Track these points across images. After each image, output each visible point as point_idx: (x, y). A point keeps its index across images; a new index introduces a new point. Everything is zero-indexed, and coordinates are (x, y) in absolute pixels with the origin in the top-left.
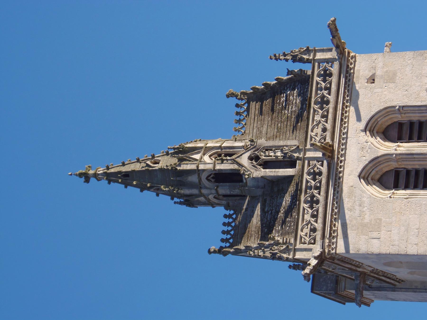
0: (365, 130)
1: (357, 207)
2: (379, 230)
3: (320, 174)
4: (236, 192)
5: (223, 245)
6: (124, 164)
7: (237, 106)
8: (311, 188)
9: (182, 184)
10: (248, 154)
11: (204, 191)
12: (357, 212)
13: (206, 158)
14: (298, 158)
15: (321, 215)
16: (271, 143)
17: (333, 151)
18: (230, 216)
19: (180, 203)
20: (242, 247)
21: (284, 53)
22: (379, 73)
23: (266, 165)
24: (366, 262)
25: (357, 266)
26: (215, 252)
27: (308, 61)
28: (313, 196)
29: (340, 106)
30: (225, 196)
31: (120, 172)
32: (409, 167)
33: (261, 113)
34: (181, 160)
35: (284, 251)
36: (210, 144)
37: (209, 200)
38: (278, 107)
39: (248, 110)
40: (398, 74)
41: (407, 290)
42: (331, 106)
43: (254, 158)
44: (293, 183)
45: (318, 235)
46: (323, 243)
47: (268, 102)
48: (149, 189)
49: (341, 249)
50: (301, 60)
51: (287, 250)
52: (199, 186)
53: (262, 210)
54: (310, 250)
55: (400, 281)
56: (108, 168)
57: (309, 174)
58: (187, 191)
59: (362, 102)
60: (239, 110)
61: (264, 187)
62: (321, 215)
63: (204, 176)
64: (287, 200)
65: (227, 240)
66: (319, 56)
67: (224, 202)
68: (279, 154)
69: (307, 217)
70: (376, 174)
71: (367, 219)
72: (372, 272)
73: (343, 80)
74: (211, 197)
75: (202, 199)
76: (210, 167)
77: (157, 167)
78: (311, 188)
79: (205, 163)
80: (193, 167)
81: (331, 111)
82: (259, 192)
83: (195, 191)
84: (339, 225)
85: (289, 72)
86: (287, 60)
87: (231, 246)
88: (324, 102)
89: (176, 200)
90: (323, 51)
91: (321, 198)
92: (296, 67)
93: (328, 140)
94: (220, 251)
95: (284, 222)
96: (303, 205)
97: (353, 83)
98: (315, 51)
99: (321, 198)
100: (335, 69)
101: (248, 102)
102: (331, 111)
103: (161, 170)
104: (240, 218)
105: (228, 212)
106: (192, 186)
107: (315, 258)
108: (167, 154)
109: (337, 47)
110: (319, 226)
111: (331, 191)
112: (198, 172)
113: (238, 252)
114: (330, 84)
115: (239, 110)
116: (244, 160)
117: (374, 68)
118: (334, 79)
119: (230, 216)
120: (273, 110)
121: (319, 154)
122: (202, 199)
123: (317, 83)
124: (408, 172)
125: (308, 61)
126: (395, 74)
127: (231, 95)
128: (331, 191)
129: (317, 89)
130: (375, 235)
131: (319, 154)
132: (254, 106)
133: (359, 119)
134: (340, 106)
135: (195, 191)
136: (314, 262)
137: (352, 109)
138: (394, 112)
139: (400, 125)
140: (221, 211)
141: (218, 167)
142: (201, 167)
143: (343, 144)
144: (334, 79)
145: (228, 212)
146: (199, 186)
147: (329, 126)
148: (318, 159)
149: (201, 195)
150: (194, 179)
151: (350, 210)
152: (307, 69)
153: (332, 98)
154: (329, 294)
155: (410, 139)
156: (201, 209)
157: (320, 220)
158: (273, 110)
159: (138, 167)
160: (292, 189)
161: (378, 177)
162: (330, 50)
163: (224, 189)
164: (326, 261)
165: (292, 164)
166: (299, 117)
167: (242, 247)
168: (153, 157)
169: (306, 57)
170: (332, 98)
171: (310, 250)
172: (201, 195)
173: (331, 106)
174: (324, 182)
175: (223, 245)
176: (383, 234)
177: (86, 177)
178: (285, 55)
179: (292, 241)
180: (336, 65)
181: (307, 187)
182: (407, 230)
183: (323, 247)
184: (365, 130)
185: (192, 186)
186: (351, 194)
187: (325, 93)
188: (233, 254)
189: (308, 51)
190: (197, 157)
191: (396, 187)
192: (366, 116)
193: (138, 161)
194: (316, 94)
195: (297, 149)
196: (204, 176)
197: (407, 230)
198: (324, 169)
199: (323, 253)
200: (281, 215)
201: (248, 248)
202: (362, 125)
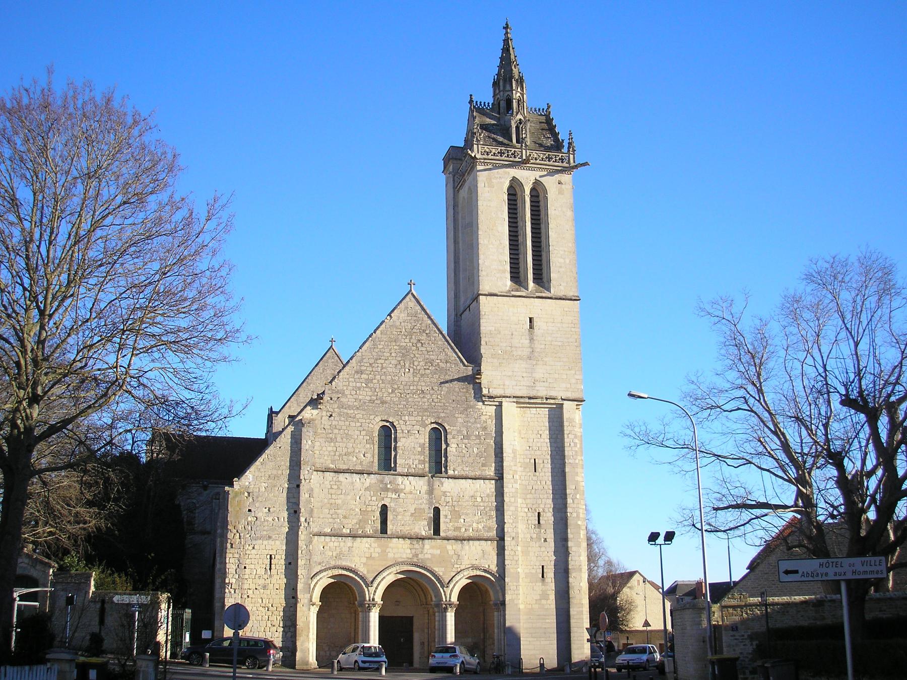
0: (536, 179)
1: (499, 176)
2: (489, 187)
3: (515, 157)
4: (502, 110)
5: (475, 102)
6: (513, 48)
7: (543, 109)
8: (508, 152)
9: (505, 81)
10: (522, 118)
11: (502, 93)
12: (497, 176)
13: (518, 94)
14: (522, 146)
15: (495, 157)
16: (528, 131)
17: (526, 164)
18: (489, 106)
19: (494, 79)
20: (475, 114)
21: (504, 28)
22: (563, 186)
23: (517, 128)
24: (471, 178)
25: (468, 173)
26: (471, 98)
27: (569, 151)
28: (504, 153)
29: (547, 167)
30: (499, 103)
31: (509, 47)
32: (518, 201)
33: (540, 123)
34: (517, 81)
35: (477, 139)
36: (525, 96)
37: (497, 95)
38: (544, 132)
39: (541, 115)
40: (563, 196)
41: (454, 195)
42: (547, 163)
43: (520, 121)
44: (509, 142)
45: (485, 156)
46: (482, 159)
47: (546, 126)
48: (501, 62)
49: (479, 168)
50: (569, 148)
51: (478, 141)
52: (504, 90)
53: (494, 124)
54: (478, 152)
55: (458, 191)
56: (511, 40)
57: (515, 151)
58: (501, 83)
59: (548, 177)
60: (541, 110)
61: (505, 125)
62: (495, 157)
63: (509, 93)
64: (501, 139)
65: (477, 104)
66: (571, 156)
67: (496, 103)
68: (524, 136)
69: (494, 151)
70: (515, 185)
71: (494, 181)
72: (465, 180)
73: (560, 168)
74: (498, 96)
75: (497, 91)
76: (514, 97)
77: (513, 68)
78: (508, 152)
79: (516, 94)
80: (514, 88)
81: (545, 162)
82: (502, 122)
83: (501, 88)
84: (490, 167)
85: (563, 140)
86: (569, 139)
87: (474, 107)
88: (549, 159)
89: (496, 77)
90: (574, 158)
91: (503, 158)
92: (566, 144)
93: (532, 161)
94: (471, 102)
95: (489, 137)
96: (500, 148)
97: (558, 174)
98: (574, 154)
99: (503, 158)
100: (565, 164)
101: (545, 115)
102: (545, 162)
103: (512, 70)
104: (488, 111)
105: (490, 104)
106: (504, 87)
107: (475, 156)
108: (520, 73)
109: (576, 166)
110: (490, 157)
111: (507, 163)
112: (512, 90)
113: (471, 111)
114: (558, 162)
115: (541, 110)
116: (519, 117)
117: (565, 184)
118: (560, 164)
119: (489, 106)
120: (542, 129)
121: (524, 157)
122: (497, 91)
123: (558, 156)
124: (516, 200)
125: (569, 151)
126: (563, 194)
127: (549, 107)
128: (507, 163)
129: (555, 155)
130: (486, 185)
131: (524, 158)
132: (543, 119)
133: (541, 177)
134: (547, 167)
135: (501, 88)
136: (473, 155)
137: (546, 173)
138: (544, 194)
139: (538, 196)
140: (491, 101)
141: (514, 101)
142: (514, 92)
143: (529, 169)
144: (560, 164)
145: (490, 104)
146: (504, 90)
147: (538, 161)
148: (522, 156)
149: (500, 92)
150: (508, 88)
151: (497, 172)
152: (565, 150)
153: (551, 163)
154: (449, 155)
155: (531, 201)
156: (492, 90)
157: (493, 157)
158: (542, 129)
159: (512, 57)
160: (506, 141)
161: (513, 185)
162: (574, 162)
163: (503, 104)
164: (899, 405)
165: (518, 142)
166: (541, 145)
167: (475, 114)
168: (518, 65)
169: (571, 150)
170: (551, 163)
171: (478, 152)
172: (500, 92)
173: (547, 163)
174: (511, 159)
175: (475, 102)
176: (487, 189)
177: (506, 27)
178: (572, 138)
179: (481, 143)
180: (567, 165)
181: (508, 150)
182: (489, 200)
183: (480, 159)
184: (536, 179)
185: (504, 87)
186: (506, 173)
187: (554, 160)
188: (470, 108)
189: (574, 151)
190: (519, 90)
191: (509, 194)
192: (542, 180)
193: (515, 57)
194: (553, 155)
195: (526, 145)
196: (509, 93)
197: (489, 200)
198: (517, 159)
199: (477, 159)
200: (493, 136)
201: (474, 118)
202: (538, 178)
